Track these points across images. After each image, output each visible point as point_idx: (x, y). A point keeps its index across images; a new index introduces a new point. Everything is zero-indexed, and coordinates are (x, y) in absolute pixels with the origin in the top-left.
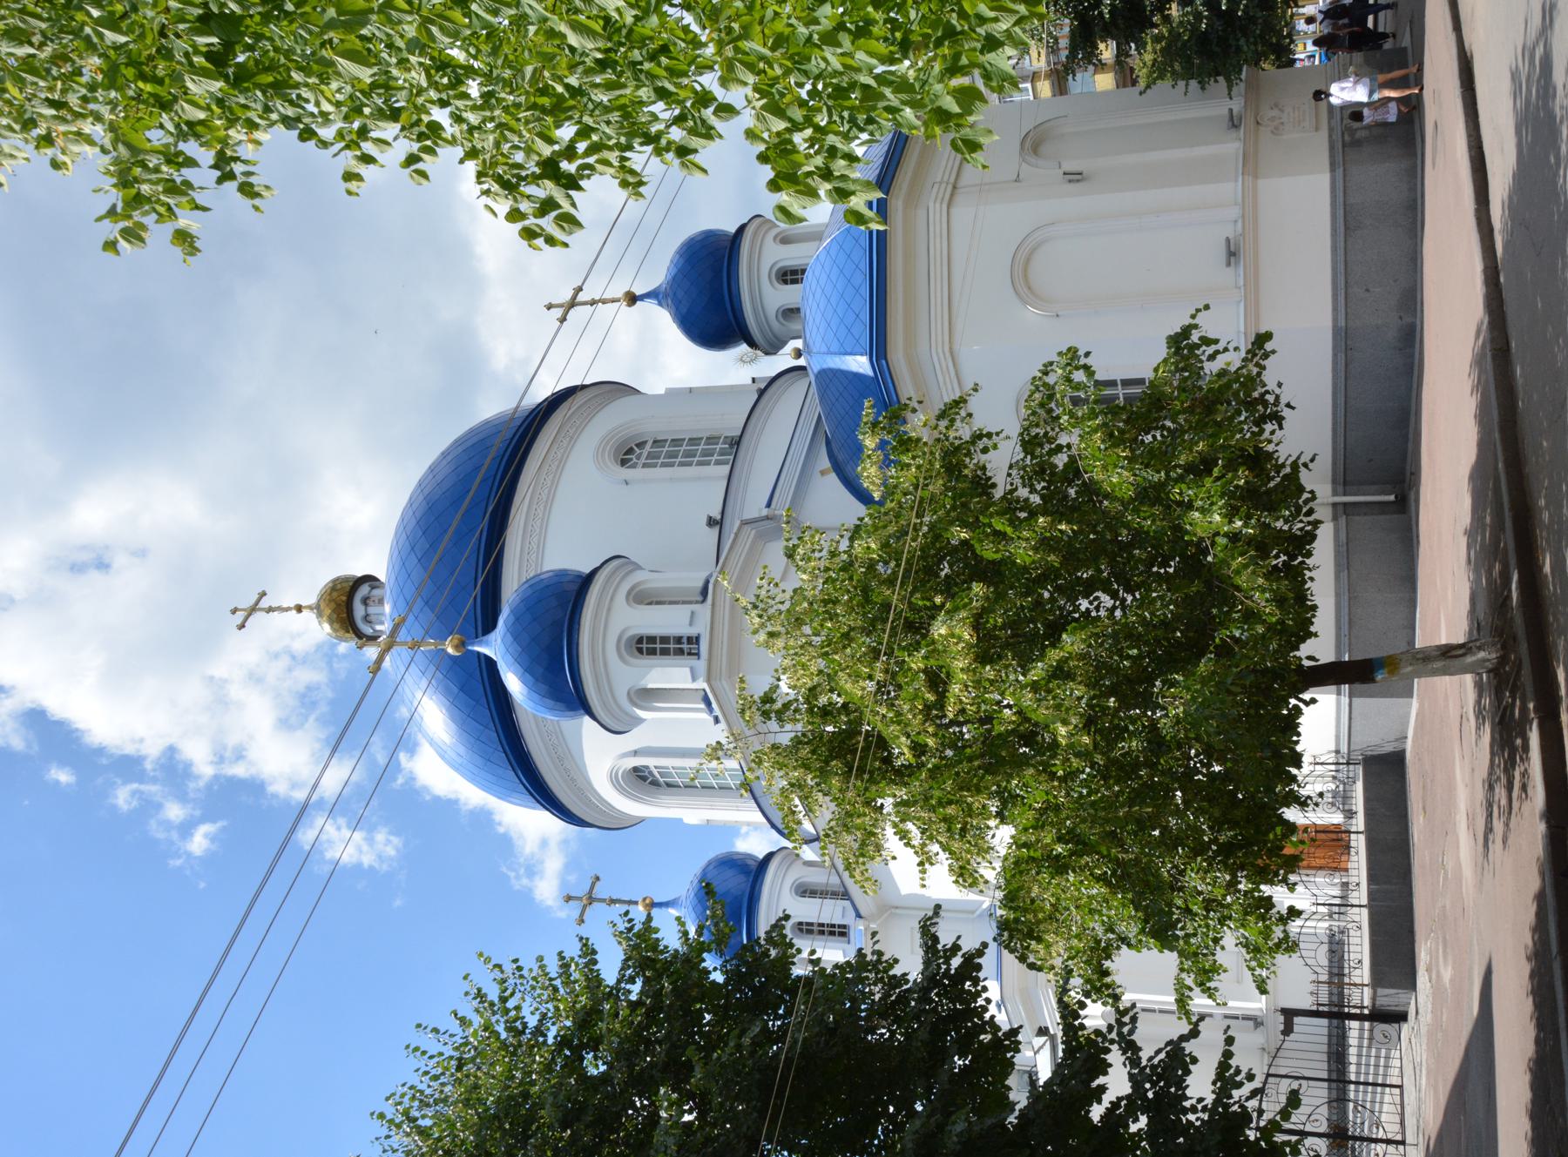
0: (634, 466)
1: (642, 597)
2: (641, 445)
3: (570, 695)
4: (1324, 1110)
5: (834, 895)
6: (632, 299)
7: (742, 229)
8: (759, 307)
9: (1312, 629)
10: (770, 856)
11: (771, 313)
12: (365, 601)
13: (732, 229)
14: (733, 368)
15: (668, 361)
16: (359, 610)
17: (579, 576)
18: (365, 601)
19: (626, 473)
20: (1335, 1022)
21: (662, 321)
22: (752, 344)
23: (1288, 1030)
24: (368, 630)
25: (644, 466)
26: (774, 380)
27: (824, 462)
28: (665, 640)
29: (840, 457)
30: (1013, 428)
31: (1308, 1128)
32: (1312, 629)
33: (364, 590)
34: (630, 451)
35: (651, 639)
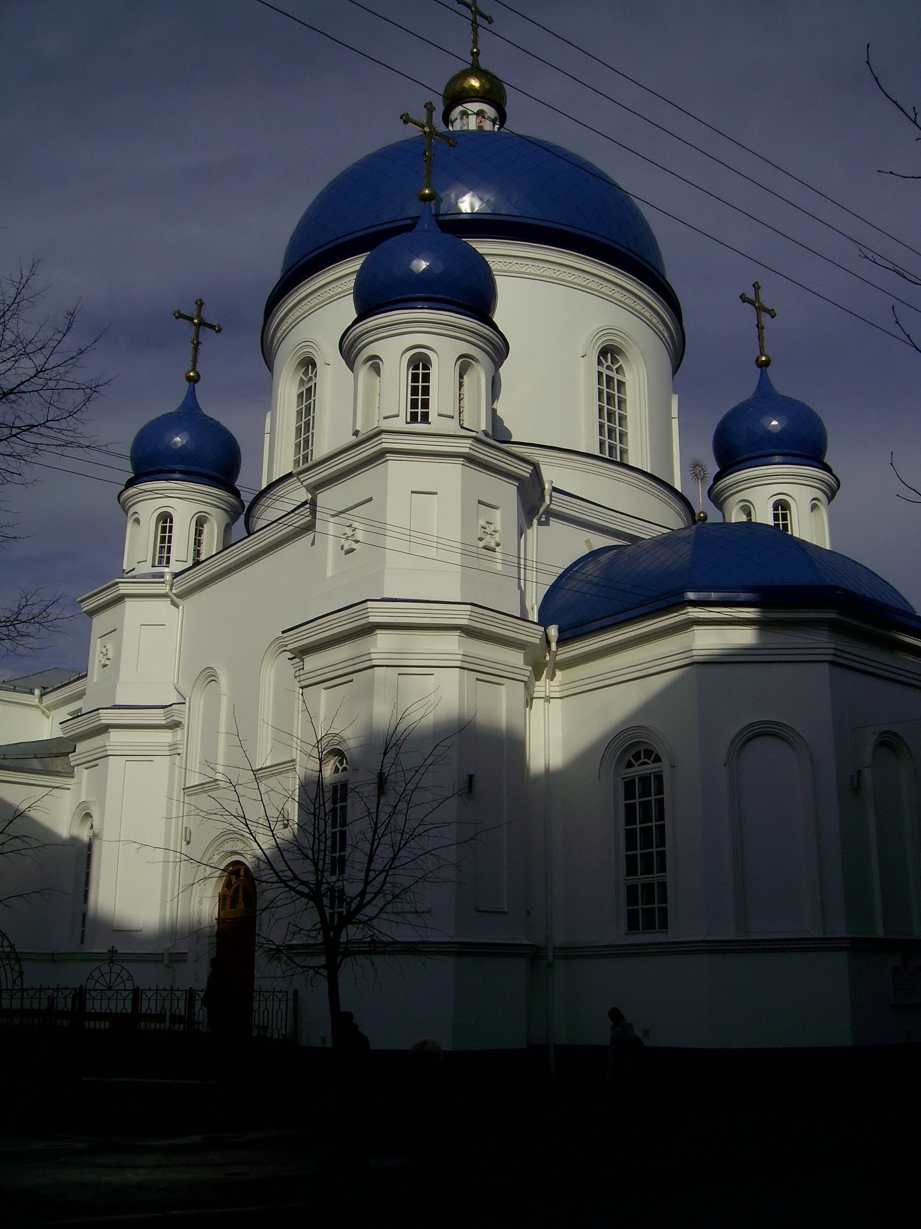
0: (600, 363)
2: (619, 370)
3: (370, 301)
5: (197, 553)
7: (494, 326)
10: (236, 493)
22: (718, 478)
25: (600, 374)
27: (600, 541)
33: (490, 111)
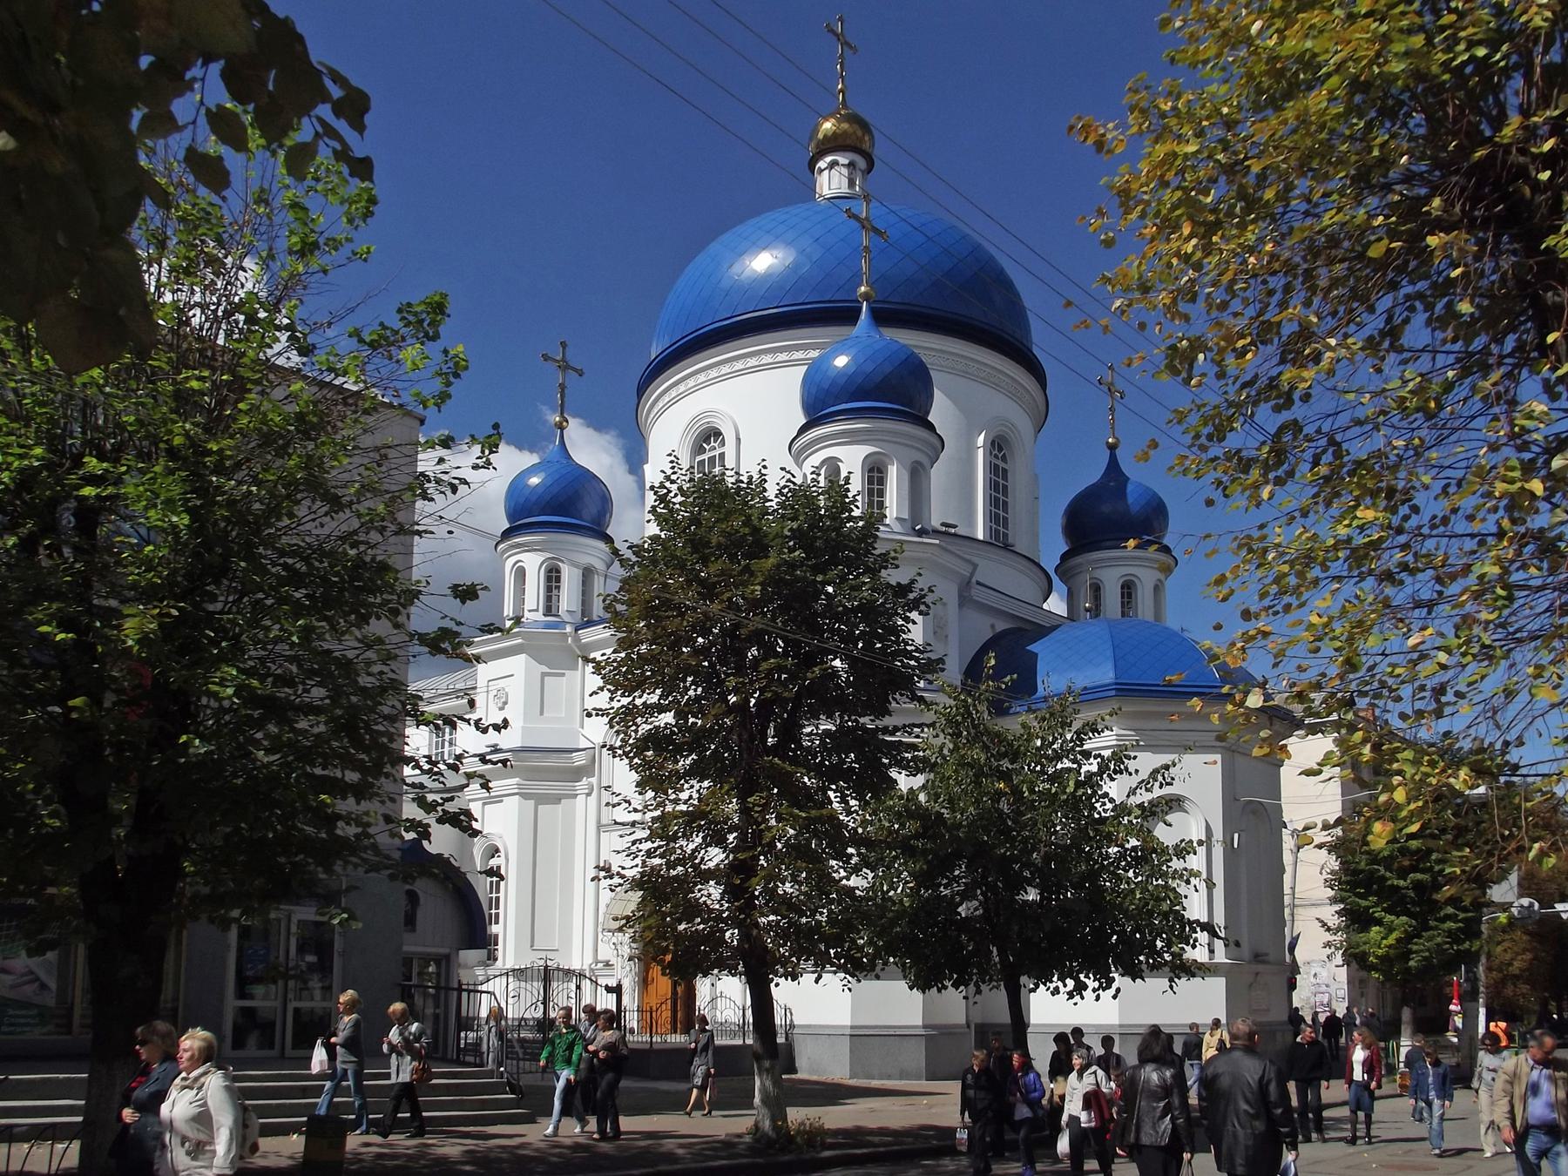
14: (1052, 548)
22: (1065, 557)
27: (1001, 626)
33: (861, 163)
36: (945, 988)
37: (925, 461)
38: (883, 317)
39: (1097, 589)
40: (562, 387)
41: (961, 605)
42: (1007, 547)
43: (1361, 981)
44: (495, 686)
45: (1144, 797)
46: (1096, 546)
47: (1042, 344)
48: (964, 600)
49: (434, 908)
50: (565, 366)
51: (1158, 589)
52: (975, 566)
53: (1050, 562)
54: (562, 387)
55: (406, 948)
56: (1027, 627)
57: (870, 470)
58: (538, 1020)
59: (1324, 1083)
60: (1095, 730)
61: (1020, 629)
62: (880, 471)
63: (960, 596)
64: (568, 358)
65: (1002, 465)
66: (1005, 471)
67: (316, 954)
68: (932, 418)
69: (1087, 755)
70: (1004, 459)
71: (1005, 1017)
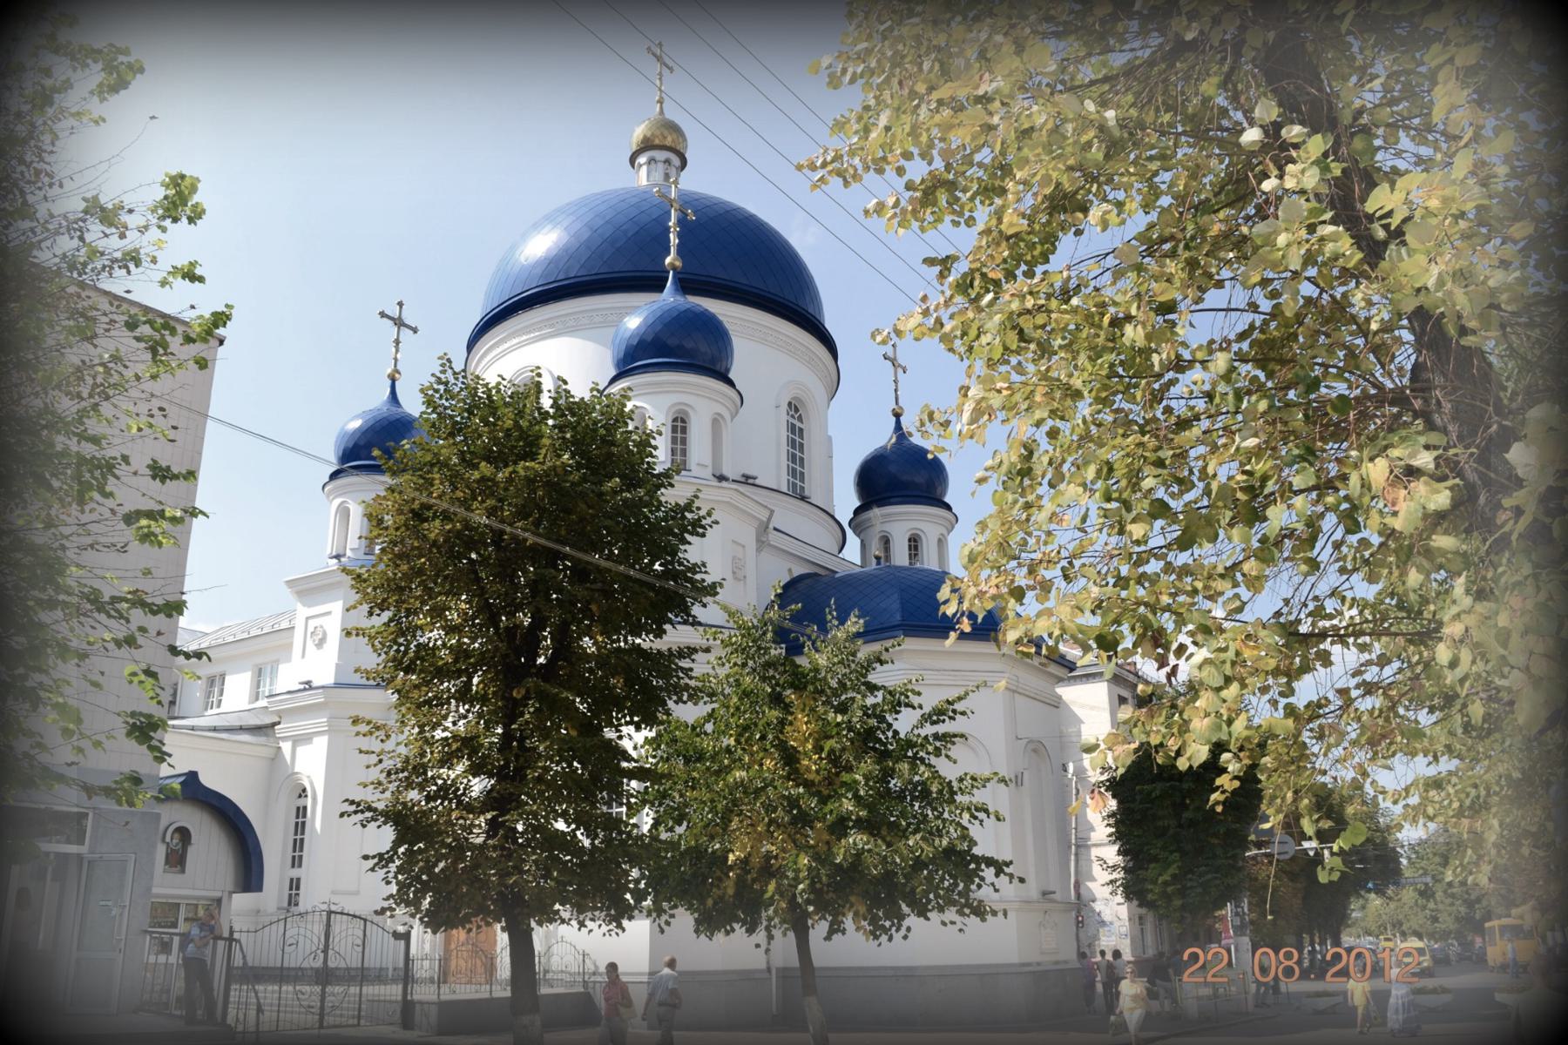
1: (716, 422)
4: (343, 965)
6: (897, 415)
8: (887, 519)
9: (625, 923)
11: (887, 527)
12: (667, 162)
13: (947, 499)
14: (846, 501)
15: (852, 436)
16: (661, 155)
17: (728, 370)
18: (667, 162)
19: (785, 407)
20: (402, 974)
21: (881, 437)
22: (857, 512)
23: (396, 936)
24: (642, 159)
26: (833, 517)
27: (799, 570)
28: (684, 442)
29: (801, 586)
30: (974, 800)
31: (330, 952)
32: (625, 923)
33: (676, 161)
34: (797, 410)
35: (684, 430)
36: (733, 930)
37: (727, 416)
38: (687, 285)
39: (886, 542)
40: (397, 342)
41: (759, 550)
42: (803, 498)
43: (1141, 918)
44: (312, 624)
45: (929, 730)
46: (883, 502)
47: (830, 324)
48: (761, 543)
49: (210, 850)
50: (399, 323)
51: (941, 542)
52: (772, 512)
53: (844, 513)
54: (397, 342)
55: (155, 890)
56: (822, 572)
57: (675, 420)
58: (317, 970)
59: (544, 990)
60: (882, 663)
61: (816, 574)
62: (683, 421)
63: (758, 541)
64: (404, 316)
65: (798, 424)
66: (801, 430)
67: (1148, 1019)
68: (731, 375)
69: (872, 688)
70: (800, 419)
71: (794, 961)
